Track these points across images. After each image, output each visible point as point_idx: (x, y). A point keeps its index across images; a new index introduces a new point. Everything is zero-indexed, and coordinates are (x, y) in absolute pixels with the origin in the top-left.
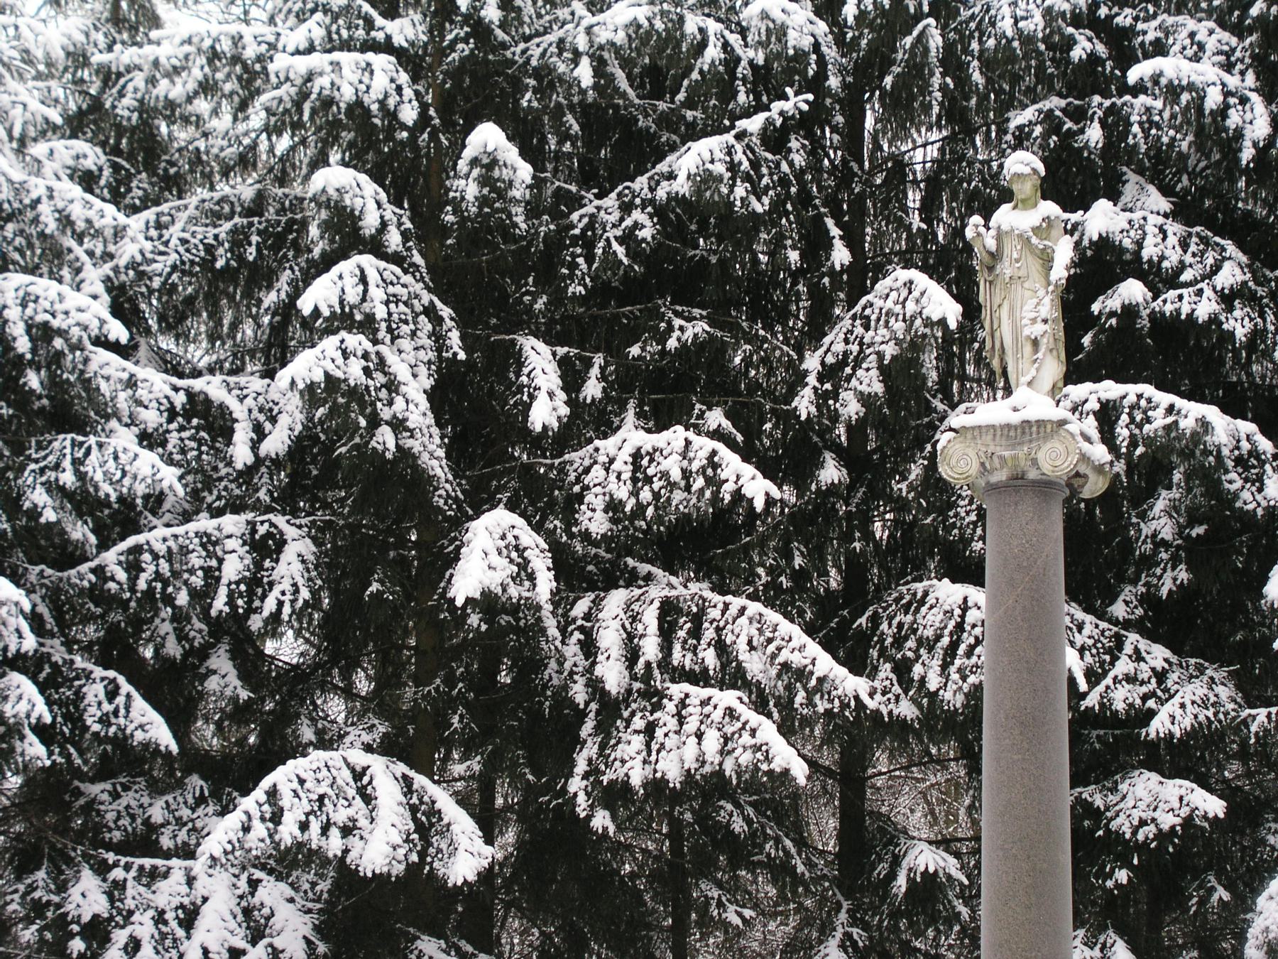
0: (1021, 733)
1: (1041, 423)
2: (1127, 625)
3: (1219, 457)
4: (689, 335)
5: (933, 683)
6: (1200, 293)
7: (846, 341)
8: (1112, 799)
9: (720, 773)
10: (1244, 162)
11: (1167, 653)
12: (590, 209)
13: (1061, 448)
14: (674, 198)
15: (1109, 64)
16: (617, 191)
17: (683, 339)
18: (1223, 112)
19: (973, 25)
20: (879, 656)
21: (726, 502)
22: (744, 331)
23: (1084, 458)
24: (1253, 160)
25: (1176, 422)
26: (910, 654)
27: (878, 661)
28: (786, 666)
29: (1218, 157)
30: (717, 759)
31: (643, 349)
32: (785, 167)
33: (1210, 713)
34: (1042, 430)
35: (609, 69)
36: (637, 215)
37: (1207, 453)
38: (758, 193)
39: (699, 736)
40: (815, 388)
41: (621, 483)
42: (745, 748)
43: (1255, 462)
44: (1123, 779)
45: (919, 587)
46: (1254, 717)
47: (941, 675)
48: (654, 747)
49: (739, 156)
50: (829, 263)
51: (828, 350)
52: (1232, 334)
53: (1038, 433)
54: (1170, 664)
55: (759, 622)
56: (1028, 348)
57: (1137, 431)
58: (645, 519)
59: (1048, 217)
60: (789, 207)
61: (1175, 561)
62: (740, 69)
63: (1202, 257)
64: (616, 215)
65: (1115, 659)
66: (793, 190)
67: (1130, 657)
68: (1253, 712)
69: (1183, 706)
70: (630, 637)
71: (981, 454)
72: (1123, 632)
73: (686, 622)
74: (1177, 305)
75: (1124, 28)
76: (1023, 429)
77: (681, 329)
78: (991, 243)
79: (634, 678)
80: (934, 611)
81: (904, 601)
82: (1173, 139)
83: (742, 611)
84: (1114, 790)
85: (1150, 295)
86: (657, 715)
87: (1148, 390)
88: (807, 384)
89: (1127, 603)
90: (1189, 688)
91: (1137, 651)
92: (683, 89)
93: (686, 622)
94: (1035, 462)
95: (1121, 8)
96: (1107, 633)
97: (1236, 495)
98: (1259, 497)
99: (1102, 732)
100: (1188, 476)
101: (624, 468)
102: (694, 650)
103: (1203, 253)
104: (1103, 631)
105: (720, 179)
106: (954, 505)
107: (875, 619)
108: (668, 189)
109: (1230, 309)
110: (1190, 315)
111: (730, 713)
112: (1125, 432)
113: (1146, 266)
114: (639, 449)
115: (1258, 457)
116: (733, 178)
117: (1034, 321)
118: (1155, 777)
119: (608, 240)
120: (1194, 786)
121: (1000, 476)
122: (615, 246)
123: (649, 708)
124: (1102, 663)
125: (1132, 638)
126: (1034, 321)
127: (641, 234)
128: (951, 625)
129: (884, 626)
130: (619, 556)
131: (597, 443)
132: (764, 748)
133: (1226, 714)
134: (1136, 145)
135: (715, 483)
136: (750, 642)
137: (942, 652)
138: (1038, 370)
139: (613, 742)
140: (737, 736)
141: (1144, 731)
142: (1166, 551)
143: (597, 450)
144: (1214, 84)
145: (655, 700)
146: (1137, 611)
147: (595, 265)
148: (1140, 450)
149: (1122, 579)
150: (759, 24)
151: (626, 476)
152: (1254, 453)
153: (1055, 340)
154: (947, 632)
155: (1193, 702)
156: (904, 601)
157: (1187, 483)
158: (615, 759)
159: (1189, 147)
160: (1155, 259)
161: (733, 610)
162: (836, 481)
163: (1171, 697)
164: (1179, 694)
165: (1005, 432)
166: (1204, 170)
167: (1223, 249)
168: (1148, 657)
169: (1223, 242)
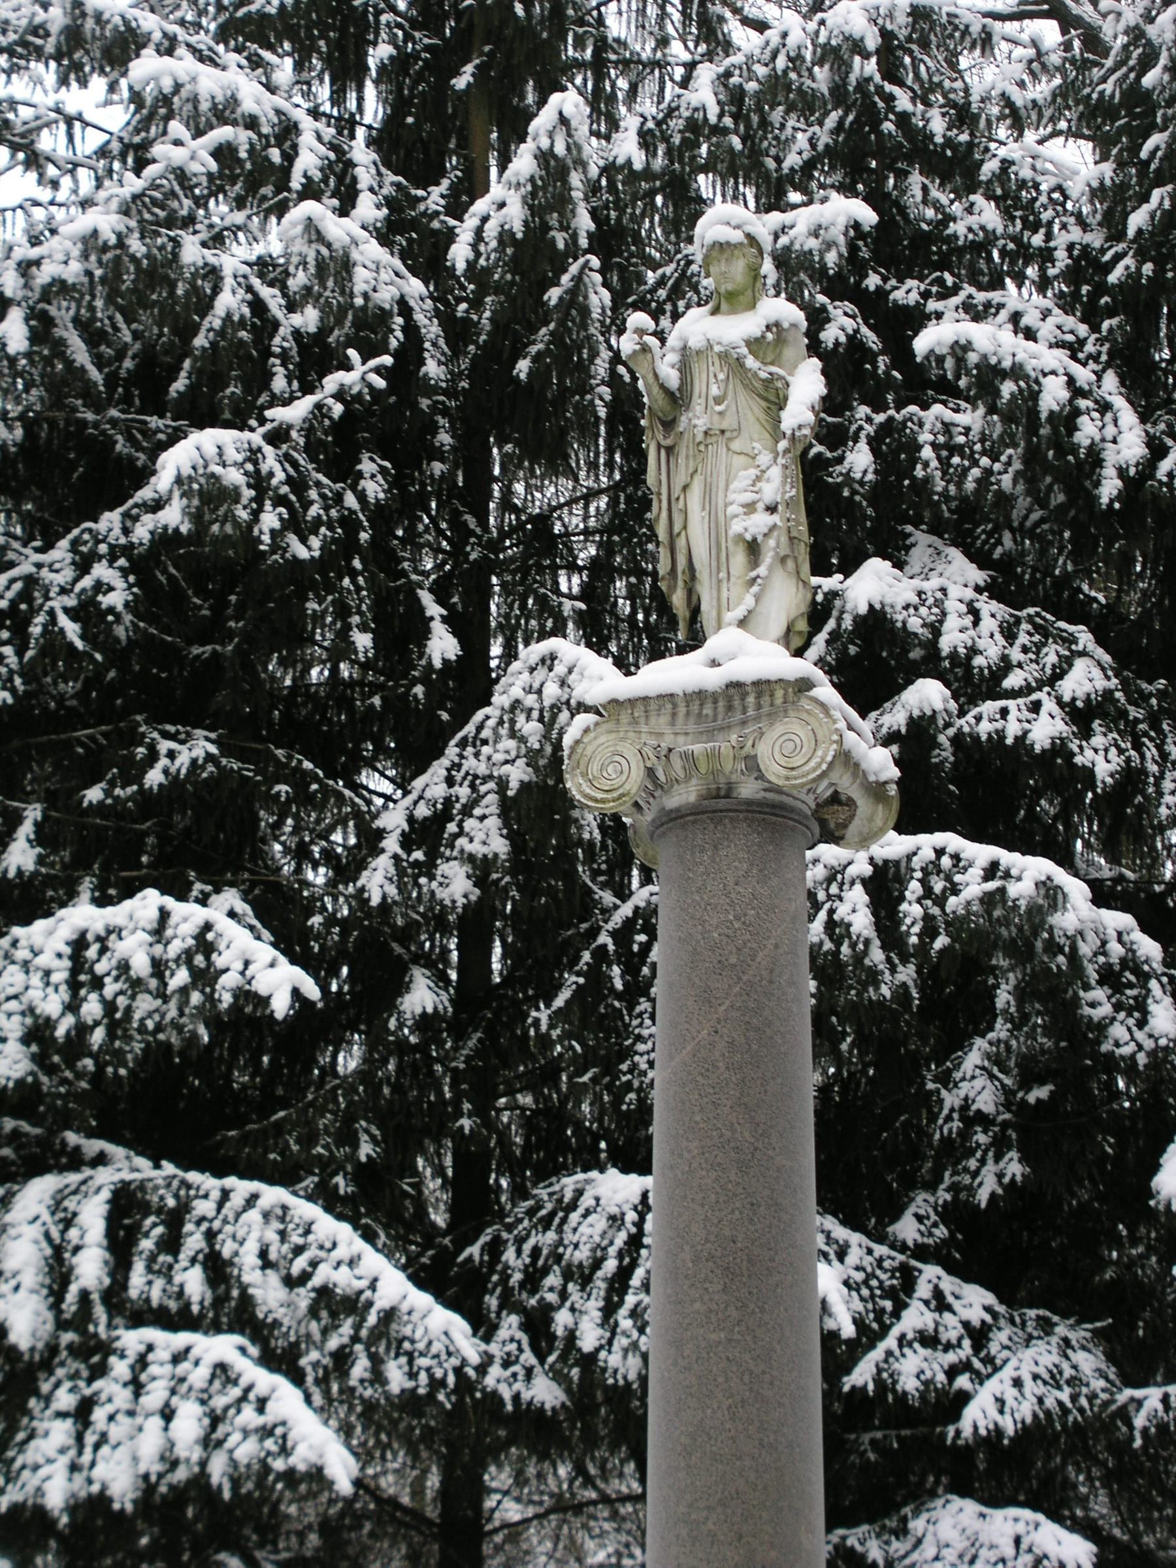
0: (725, 1289)
1: (762, 686)
2: (922, 1253)
3: (1074, 957)
4: (184, 760)
5: (589, 1338)
6: (1036, 707)
7: (450, 781)
8: (898, 1547)
9: (201, 1478)
10: (1105, 500)
11: (990, 1298)
12: (26, 568)
13: (802, 732)
14: (165, 540)
15: (882, 362)
16: (70, 536)
17: (173, 770)
18: (1067, 420)
19: (662, 293)
20: (501, 1307)
21: (225, 1005)
22: (278, 761)
23: (845, 759)
24: (1119, 498)
25: (1002, 891)
26: (552, 1297)
27: (498, 1314)
28: (325, 1293)
29: (1061, 498)
30: (196, 1454)
31: (108, 793)
32: (350, 500)
33: (1065, 1395)
34: (766, 700)
35: (58, 332)
36: (101, 571)
37: (1053, 948)
38: (296, 525)
39: (168, 1414)
40: (395, 857)
41: (50, 990)
42: (246, 1433)
43: (1132, 978)
44: (917, 1513)
45: (568, 1184)
46: (1139, 1403)
47: (602, 1326)
48: (90, 1439)
49: (270, 460)
50: (423, 662)
51: (421, 797)
52: (1088, 774)
53: (759, 707)
54: (995, 1315)
55: (282, 1219)
56: (739, 559)
57: (935, 911)
58: (90, 1055)
59: (777, 324)
60: (357, 564)
61: (1000, 1147)
62: (277, 340)
63: (1037, 653)
64: (68, 574)
65: (900, 1308)
66: (364, 536)
67: (926, 1303)
68: (1138, 1393)
69: (1017, 1383)
70: (58, 1250)
71: (647, 750)
72: (913, 1263)
73: (155, 1225)
74: (999, 725)
75: (906, 307)
76: (730, 699)
77: (171, 755)
78: (672, 377)
79: (62, 1325)
80: (592, 1218)
81: (543, 1212)
82: (988, 472)
83: (252, 1200)
84: (901, 1531)
85: (953, 706)
86: (98, 1384)
87: (952, 841)
88: (383, 851)
89: (919, 1218)
90: (1028, 1354)
91: (938, 1294)
92: (183, 374)
93: (155, 1225)
94: (752, 765)
95: (901, 281)
96: (887, 1264)
97: (1101, 1027)
98: (1140, 1035)
99: (879, 1435)
100: (1020, 993)
101: (56, 963)
102: (167, 1273)
103: (1039, 646)
104: (880, 1261)
105: (233, 495)
106: (629, 1053)
107: (495, 1248)
108: (151, 526)
109: (1086, 734)
110: (1021, 739)
111: (221, 1370)
112: (916, 910)
113: (947, 664)
114: (83, 934)
115: (1137, 971)
116: (259, 500)
117: (750, 508)
118: (970, 1507)
119: (52, 613)
120: (1040, 1517)
121: (685, 795)
122: (64, 621)
123: (85, 1373)
124: (879, 1313)
125: (930, 1274)
126: (750, 508)
127: (106, 600)
128: (621, 1238)
129: (509, 1255)
130: (53, 1132)
131: (17, 931)
132: (279, 1431)
133: (1092, 1397)
134: (927, 480)
135: (205, 977)
136: (263, 1254)
137: (603, 1285)
138: (758, 598)
139: (21, 1436)
140: (232, 1411)
141: (951, 1431)
142: (985, 1132)
143: (15, 943)
144: (1054, 373)
145: (96, 1359)
146: (937, 1232)
147: (30, 654)
148: (941, 942)
149: (911, 1183)
150: (305, 249)
151: (59, 977)
152: (1131, 962)
153: (791, 539)
154: (612, 1251)
155: (1036, 1377)
156: (543, 1212)
157: (1020, 1007)
158: (23, 1467)
159: (1015, 481)
160: (962, 651)
161: (237, 1200)
162: (430, 1010)
163: (996, 1369)
164: (1013, 1363)
165: (695, 708)
166: (1037, 524)
167: (1071, 640)
168: (956, 1305)
169: (1071, 628)
